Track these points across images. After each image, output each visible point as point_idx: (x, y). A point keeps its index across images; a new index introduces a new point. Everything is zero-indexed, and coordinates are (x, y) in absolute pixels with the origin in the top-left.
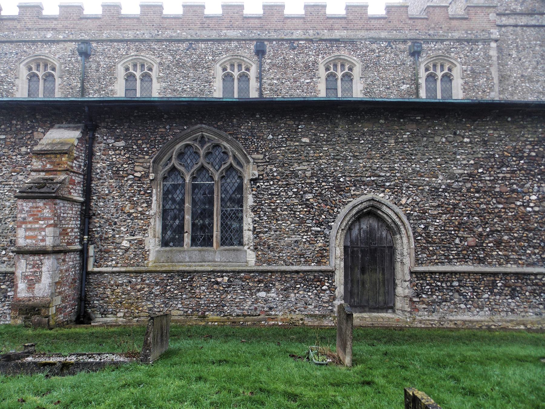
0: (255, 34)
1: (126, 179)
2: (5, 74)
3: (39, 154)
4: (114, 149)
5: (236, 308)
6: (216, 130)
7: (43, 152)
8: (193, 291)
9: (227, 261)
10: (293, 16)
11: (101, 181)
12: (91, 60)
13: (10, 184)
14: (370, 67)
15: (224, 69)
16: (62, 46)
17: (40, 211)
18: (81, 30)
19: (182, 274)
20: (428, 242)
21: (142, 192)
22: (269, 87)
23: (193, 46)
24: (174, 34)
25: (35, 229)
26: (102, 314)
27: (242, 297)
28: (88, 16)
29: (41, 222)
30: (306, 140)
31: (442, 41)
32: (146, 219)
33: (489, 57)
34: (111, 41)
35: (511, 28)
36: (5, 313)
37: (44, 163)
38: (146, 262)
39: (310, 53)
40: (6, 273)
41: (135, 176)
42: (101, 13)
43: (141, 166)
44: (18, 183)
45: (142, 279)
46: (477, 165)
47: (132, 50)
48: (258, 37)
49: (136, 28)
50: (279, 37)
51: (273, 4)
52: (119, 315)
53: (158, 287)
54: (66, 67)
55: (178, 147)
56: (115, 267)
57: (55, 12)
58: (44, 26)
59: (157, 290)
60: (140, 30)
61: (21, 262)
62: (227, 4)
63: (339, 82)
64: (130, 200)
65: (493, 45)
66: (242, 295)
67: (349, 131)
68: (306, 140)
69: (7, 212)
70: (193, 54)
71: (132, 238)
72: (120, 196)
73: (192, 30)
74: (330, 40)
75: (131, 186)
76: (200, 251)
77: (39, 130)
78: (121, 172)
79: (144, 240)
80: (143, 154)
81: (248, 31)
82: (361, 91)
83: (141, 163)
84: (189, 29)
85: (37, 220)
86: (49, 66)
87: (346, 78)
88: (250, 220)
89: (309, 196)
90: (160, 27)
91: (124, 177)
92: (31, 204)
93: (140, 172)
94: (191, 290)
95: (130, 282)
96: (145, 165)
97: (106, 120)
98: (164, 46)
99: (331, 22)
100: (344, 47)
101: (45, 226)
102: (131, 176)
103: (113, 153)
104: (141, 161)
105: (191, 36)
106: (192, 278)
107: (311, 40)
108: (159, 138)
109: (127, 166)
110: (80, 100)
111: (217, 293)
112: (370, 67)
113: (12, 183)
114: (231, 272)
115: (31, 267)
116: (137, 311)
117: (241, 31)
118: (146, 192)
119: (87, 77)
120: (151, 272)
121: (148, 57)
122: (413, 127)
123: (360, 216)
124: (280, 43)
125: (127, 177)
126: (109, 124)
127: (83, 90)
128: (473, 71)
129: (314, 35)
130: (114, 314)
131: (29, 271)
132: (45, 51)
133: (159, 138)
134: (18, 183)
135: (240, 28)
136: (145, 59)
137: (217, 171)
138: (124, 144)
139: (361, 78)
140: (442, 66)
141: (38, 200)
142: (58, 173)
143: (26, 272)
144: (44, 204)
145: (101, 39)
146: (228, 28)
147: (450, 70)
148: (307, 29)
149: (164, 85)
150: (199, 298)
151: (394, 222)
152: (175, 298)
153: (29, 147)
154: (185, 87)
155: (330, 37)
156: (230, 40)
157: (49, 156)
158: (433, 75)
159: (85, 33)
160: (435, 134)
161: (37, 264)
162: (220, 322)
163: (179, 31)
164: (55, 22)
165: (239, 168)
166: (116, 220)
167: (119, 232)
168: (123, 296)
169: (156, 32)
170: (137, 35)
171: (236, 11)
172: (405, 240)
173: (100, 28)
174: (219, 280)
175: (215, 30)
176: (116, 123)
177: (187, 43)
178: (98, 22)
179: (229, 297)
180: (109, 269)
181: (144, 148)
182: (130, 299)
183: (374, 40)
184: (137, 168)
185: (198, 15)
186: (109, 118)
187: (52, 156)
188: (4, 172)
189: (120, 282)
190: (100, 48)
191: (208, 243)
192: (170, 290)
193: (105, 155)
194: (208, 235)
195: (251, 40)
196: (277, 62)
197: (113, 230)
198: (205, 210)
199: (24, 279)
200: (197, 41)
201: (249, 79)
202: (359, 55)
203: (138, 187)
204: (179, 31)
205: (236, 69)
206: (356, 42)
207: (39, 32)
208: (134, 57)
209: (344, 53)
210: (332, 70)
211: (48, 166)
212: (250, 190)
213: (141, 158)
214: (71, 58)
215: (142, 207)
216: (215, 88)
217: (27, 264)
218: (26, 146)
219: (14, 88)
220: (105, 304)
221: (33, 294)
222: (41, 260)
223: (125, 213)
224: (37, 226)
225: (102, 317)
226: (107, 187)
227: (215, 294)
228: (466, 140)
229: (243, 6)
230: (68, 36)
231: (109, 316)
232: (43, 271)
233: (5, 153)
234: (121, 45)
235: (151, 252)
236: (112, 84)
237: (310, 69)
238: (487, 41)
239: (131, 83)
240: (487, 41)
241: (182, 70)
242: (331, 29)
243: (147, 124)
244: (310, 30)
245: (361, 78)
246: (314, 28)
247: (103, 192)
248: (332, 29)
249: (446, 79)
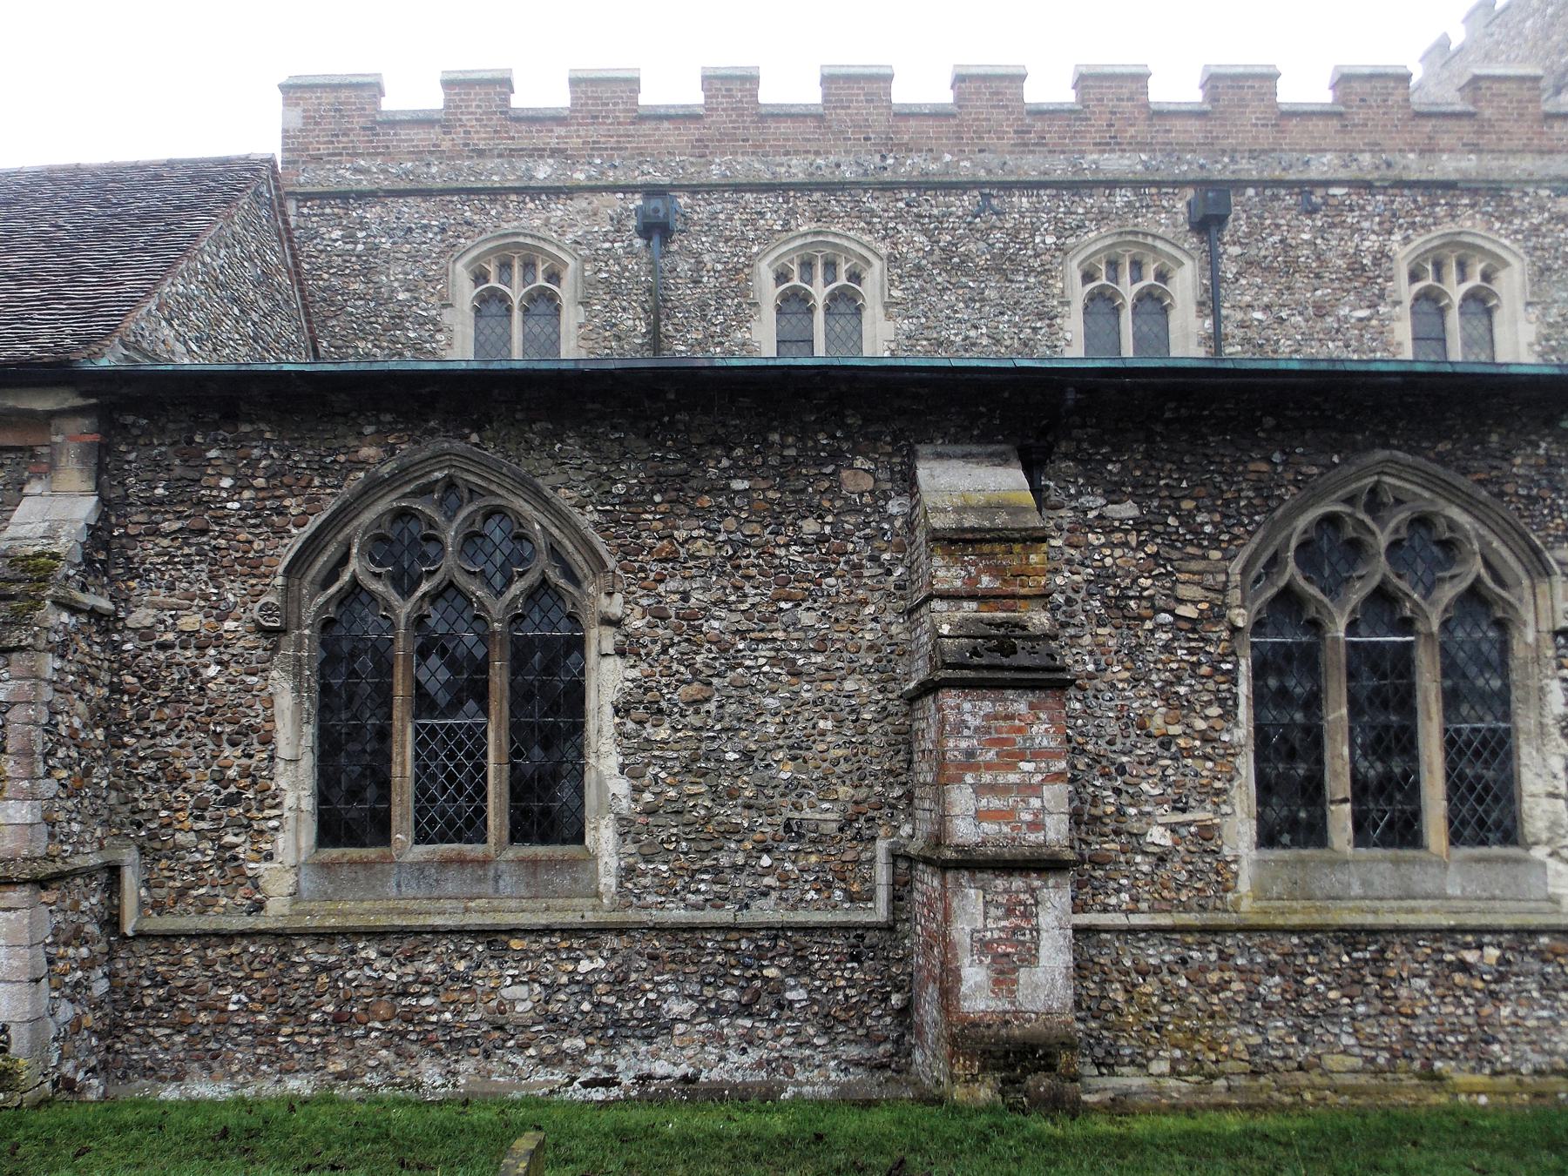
0: (1190, 163)
1: (1149, 625)
2: (408, 295)
3: (952, 542)
4: (1105, 525)
5: (1528, 1048)
6: (1437, 469)
7: (969, 536)
8: (1388, 993)
9: (1485, 895)
10: (1306, 108)
11: (1071, 631)
12: (674, 247)
13: (774, 640)
14: (1556, 271)
15: (480, 277)
16: (584, 204)
17: (1019, 730)
18: (641, 154)
19: (1351, 936)
21: (1205, 670)
22: (1239, 333)
23: (995, 202)
24: (933, 167)
25: (1006, 789)
26: (1098, 1066)
27: (1545, 1013)
28: (662, 111)
29: (1027, 766)
32: (1223, 756)
34: (739, 188)
36: (786, 1058)
37: (972, 569)
38: (1230, 896)
39: (1366, 225)
40: (782, 928)
41: (1178, 617)
42: (701, 100)
43: (1198, 584)
44: (801, 635)
45: (1220, 952)
47: (802, 215)
48: (1204, 175)
49: (813, 147)
50: (1266, 175)
51: (1241, 70)
52: (1155, 1067)
53: (1277, 979)
54: (600, 270)
55: (368, 517)
56: (1132, 912)
57: (558, 98)
58: (525, 143)
59: (1272, 987)
60: (828, 152)
61: (966, 896)
62: (1099, 70)
63: (819, 316)
66: (1543, 1007)
69: (771, 729)
70: (993, 227)
71: (1181, 817)
72: (1134, 681)
73: (991, 152)
74: (1428, 186)
75: (1167, 648)
76: (1396, 862)
77: (858, 463)
78: (1132, 603)
79: (1218, 827)
80: (1200, 546)
81: (1169, 155)
82: (1530, 345)
83: (1194, 573)
84: (981, 151)
85: (1011, 759)
86: (541, 268)
90: (889, 145)
91: (1142, 619)
92: (987, 707)
93: (1195, 603)
94: (1383, 988)
95: (1184, 961)
96: (1209, 580)
97: (1075, 432)
98: (901, 205)
99: (1428, 126)
100: (1472, 206)
101: (1038, 778)
102: (1165, 618)
103: (1103, 540)
104: (1194, 566)
105: (989, 172)
106: (1382, 951)
107: (1367, 186)
108: (1251, 494)
109: (1149, 581)
110: (307, 368)
111: (1467, 1001)
112: (1556, 271)
113: (780, 635)
114: (1508, 932)
115: (1000, 912)
116: (1213, 1057)
117: (1144, 157)
118: (1216, 669)
119: (665, 301)
120: (1250, 930)
121: (851, 237)
124: (1268, 192)
125: (1150, 619)
126: (1085, 445)
127: (656, 338)
129: (1377, 168)
130: (1140, 1063)
131: (996, 927)
132: (531, 219)
133: (1251, 494)
134: (801, 635)
135: (1141, 146)
136: (846, 243)
137: (500, 594)
138: (1135, 512)
139: (1529, 304)
140: (1137, 266)
141: (1010, 694)
142: (1020, 603)
143: (985, 929)
144: (1032, 706)
145: (704, 181)
146: (1102, 146)
147: (1162, 276)
148: (1352, 151)
149: (905, 325)
150: (1407, 1016)
152: (1330, 1013)
153: (829, 519)
154: (972, 333)
155: (1424, 177)
156: (1112, 184)
157: (986, 548)
158: (1108, 293)
159: (654, 164)
161: (1020, 903)
162: (1495, 1093)
163: (948, 157)
164: (561, 131)
165: (571, 589)
166: (1125, 759)
167: (1136, 798)
168: (1166, 1008)
169: (877, 158)
170: (819, 168)
171: (1125, 92)
173: (702, 149)
174: (1471, 956)
175: (1063, 152)
176: (1104, 444)
177: (976, 193)
178: (694, 131)
179: (1505, 1011)
180: (1118, 919)
181: (1202, 524)
182: (1189, 1018)
184: (1183, 591)
185: (1005, 107)
186: (1083, 426)
187: (998, 548)
188: (750, 601)
189: (1152, 961)
190: (702, 212)
191: (1403, 837)
192: (1314, 989)
193: (1076, 547)
194: (1403, 812)
195: (1175, 184)
196: (1263, 253)
197: (1118, 792)
198: (1387, 728)
199: (981, 953)
200: (1007, 187)
201: (558, 309)
202: (1516, 232)
203: (1191, 651)
204: (948, 157)
205: (1126, 277)
206: (1508, 190)
207: (509, 163)
208: (810, 239)
209: (1470, 224)
210: (796, 281)
211: (985, 581)
212: (1554, 663)
213: (1194, 557)
214: (613, 242)
215: (1207, 718)
216: (1068, 336)
217: (986, 903)
218: (821, 517)
219: (438, 336)
220: (1105, 1033)
221: (1013, 1003)
222: (1032, 891)
223: (1149, 735)
224: (1013, 778)
225: (1102, 1074)
226: (1091, 653)
227: (1459, 1003)
229: (637, 81)
230: (603, 173)
231: (1125, 1070)
232: (1043, 926)
233: (751, 536)
234: (767, 201)
235: (1244, 863)
236: (743, 321)
237: (1364, 276)
239: (794, 320)
241: (964, 280)
242: (1428, 150)
243: (1206, 445)
244: (1362, 151)
245: (1529, 304)
246: (1375, 147)
247: (1078, 668)
248: (1432, 151)
249: (1149, 306)
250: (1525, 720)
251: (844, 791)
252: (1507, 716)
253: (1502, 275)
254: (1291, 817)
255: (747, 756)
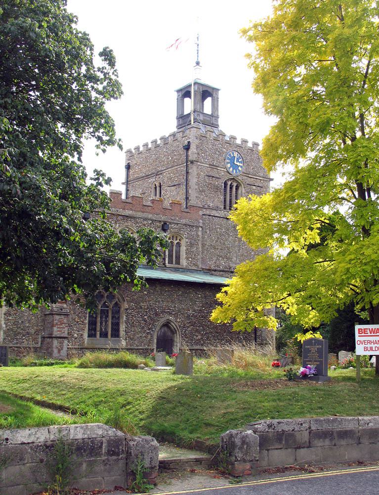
20: (186, 337)
25: (61, 328)
30: (145, 293)
31: (178, 224)
33: (198, 236)
35: (208, 216)
46: (203, 306)
64: (78, 315)
65: (200, 229)
67: (161, 289)
68: (145, 293)
72: (74, 314)
87: (178, 245)
88: (124, 327)
89: (146, 317)
107: (114, 214)
122: (182, 289)
123: (164, 325)
128: (191, 243)
151: (174, 329)
160: (190, 292)
172: (178, 336)
183: (145, 219)
228: (200, 296)
238: (197, 227)
240: (197, 227)
250: (121, 321)
251: (35, 328)
252: (119, 320)
253: (182, 240)
254: (91, 335)
255: (22, 322)
